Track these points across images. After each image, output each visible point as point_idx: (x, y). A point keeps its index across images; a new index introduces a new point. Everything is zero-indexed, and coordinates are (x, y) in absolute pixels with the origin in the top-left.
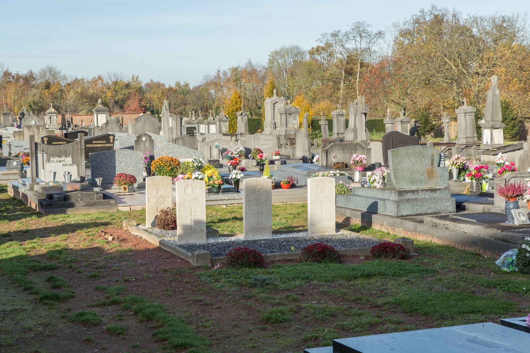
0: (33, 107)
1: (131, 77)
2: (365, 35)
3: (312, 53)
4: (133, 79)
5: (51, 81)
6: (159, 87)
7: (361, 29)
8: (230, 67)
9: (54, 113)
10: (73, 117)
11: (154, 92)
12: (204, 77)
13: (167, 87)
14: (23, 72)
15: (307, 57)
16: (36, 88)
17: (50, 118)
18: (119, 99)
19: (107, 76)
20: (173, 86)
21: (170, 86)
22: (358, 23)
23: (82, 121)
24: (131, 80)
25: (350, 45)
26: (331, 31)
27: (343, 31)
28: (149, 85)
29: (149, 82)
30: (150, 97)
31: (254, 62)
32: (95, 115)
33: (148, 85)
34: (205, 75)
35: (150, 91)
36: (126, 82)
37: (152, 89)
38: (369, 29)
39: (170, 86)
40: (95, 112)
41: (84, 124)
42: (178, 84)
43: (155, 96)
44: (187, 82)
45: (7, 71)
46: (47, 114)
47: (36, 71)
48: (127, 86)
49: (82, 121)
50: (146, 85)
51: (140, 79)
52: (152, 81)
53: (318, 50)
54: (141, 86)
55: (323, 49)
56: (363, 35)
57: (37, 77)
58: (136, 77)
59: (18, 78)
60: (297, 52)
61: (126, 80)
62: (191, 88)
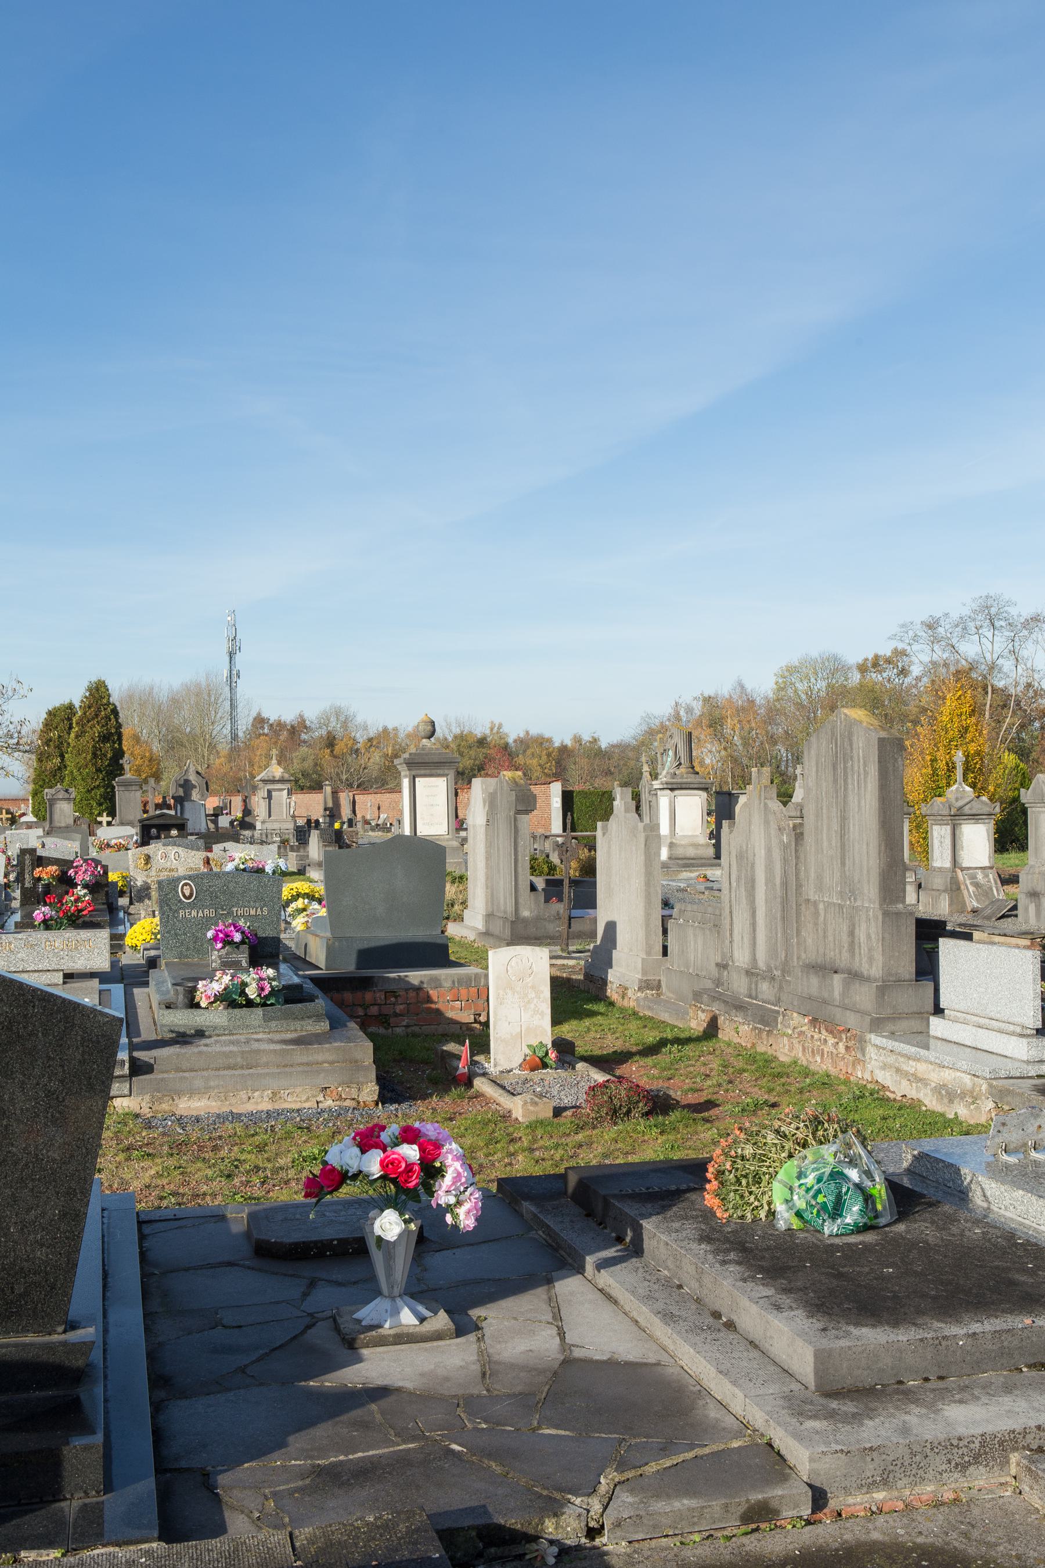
0: (302, 782)
1: (489, 725)
2: (1003, 623)
3: (862, 668)
4: (492, 729)
5: (339, 733)
6: (541, 743)
7: (993, 611)
8: (697, 694)
9: (282, 781)
10: (357, 797)
11: (533, 754)
12: (642, 718)
13: (557, 744)
14: (289, 717)
15: (856, 677)
16: (309, 746)
17: (270, 797)
18: (465, 768)
19: (444, 724)
20: (568, 742)
21: (562, 742)
22: (987, 597)
23: (379, 808)
24: (488, 732)
25: (970, 649)
26: (925, 617)
27: (955, 616)
28: (521, 742)
29: (522, 735)
30: (525, 764)
31: (749, 686)
32: (406, 783)
33: (520, 741)
34: (644, 715)
35: (525, 751)
36: (479, 736)
37: (528, 747)
38: (1013, 611)
39: (562, 742)
40: (404, 771)
41: (383, 816)
42: (577, 740)
43: (535, 761)
44: (596, 736)
45: (259, 714)
46: (261, 785)
47: (312, 714)
48: (482, 742)
49: (379, 808)
50: (515, 741)
51: (505, 729)
52: (527, 733)
53: (876, 663)
54: (507, 744)
55: (888, 661)
56: (997, 624)
57: (313, 726)
58: (497, 725)
59: (280, 725)
60: (835, 667)
61: (479, 731)
62: (603, 747)
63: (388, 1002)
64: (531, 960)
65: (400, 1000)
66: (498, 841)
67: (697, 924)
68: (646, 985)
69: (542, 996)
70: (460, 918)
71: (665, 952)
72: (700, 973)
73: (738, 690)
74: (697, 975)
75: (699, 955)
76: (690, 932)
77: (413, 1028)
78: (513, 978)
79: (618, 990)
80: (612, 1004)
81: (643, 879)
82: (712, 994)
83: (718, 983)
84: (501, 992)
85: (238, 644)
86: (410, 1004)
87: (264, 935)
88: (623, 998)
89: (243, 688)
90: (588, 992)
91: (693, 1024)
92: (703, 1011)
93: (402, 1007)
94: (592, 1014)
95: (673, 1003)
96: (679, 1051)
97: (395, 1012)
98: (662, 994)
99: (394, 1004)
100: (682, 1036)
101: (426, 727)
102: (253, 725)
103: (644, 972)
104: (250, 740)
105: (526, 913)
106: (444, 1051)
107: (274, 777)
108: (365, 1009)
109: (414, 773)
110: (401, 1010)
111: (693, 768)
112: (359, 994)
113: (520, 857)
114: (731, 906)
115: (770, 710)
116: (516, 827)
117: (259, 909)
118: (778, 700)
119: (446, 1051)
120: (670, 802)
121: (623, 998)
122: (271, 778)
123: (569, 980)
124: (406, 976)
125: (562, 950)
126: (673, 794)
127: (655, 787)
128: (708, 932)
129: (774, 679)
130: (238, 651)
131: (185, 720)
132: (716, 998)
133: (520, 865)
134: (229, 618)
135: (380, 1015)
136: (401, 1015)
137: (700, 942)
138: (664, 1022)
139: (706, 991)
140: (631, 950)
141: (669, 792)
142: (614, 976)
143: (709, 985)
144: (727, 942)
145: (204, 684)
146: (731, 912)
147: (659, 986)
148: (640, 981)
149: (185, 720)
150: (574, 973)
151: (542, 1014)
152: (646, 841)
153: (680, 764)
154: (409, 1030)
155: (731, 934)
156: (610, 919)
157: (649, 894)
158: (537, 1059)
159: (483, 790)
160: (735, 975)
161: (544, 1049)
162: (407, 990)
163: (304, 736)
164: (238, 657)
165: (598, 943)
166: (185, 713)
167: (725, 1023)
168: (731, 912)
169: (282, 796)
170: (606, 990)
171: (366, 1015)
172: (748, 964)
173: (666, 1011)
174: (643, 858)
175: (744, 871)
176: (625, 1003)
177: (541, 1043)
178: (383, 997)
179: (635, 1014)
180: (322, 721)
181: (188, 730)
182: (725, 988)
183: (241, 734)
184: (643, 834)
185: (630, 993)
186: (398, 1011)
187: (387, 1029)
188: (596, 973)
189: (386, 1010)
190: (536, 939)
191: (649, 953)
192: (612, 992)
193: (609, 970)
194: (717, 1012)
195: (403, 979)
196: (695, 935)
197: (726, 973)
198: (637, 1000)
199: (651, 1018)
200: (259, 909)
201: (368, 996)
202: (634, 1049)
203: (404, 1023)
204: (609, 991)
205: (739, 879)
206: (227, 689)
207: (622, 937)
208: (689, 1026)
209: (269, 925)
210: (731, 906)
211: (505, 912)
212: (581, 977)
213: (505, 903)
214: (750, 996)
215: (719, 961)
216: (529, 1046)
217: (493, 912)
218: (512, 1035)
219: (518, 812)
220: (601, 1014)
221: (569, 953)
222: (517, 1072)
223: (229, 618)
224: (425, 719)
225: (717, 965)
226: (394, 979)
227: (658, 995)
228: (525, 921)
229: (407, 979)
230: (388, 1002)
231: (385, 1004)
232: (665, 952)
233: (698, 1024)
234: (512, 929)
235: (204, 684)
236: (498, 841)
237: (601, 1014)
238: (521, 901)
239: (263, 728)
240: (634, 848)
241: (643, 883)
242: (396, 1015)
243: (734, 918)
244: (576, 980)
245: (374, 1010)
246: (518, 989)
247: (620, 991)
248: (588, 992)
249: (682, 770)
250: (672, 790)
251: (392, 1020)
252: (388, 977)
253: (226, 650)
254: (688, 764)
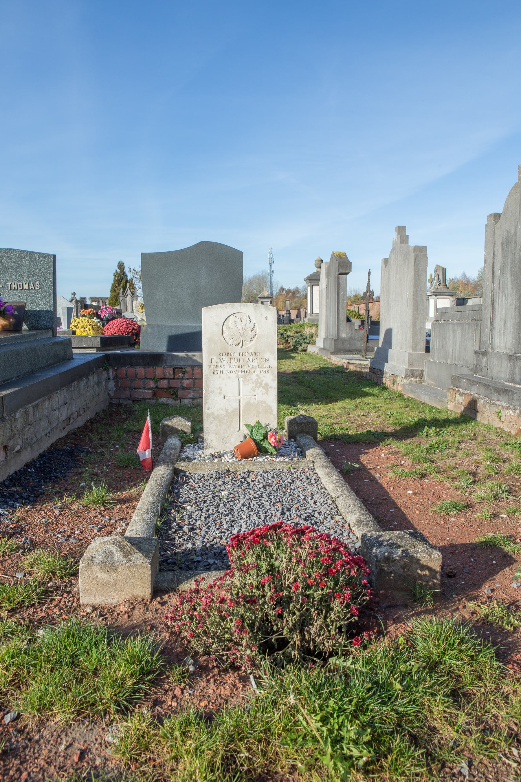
14: (292, 287)
31: (468, 275)
46: (259, 299)
59: (289, 291)
63: (176, 377)
64: (253, 320)
65: (186, 376)
67: (456, 321)
68: (411, 374)
69: (266, 365)
70: (314, 343)
71: (428, 350)
72: (456, 363)
73: (464, 276)
74: (455, 364)
75: (457, 348)
76: (450, 329)
78: (230, 342)
79: (391, 378)
80: (386, 389)
81: (412, 290)
82: (471, 378)
83: (476, 369)
84: (215, 359)
86: (195, 379)
87: (38, 309)
88: (393, 384)
89: (275, 276)
90: (371, 381)
91: (450, 406)
92: (461, 394)
93: (188, 381)
94: (367, 395)
95: (433, 388)
96: (437, 434)
97: (182, 386)
98: (423, 381)
99: (181, 379)
100: (441, 417)
103: (410, 364)
105: (343, 335)
106: (165, 426)
108: (156, 382)
110: (187, 384)
111: (446, 285)
112: (150, 369)
113: (341, 301)
114: (493, 295)
115: (475, 285)
116: (339, 283)
117: (32, 284)
118: (479, 281)
119: (168, 426)
120: (435, 301)
121: (393, 384)
123: (360, 372)
124: (194, 356)
125: (363, 356)
126: (436, 298)
127: (428, 294)
128: (466, 326)
129: (478, 273)
132: (474, 382)
133: (340, 306)
135: (169, 388)
136: (187, 389)
137: (458, 336)
138: (423, 403)
139: (464, 377)
140: (401, 348)
141: (434, 296)
142: (388, 368)
143: (466, 371)
144: (487, 331)
145: (261, 275)
146: (493, 302)
147: (421, 375)
148: (407, 370)
150: (364, 368)
151: (266, 387)
152: (415, 259)
153: (440, 284)
155: (492, 323)
156: (388, 327)
157: (417, 301)
158: (253, 444)
160: (495, 361)
161: (263, 431)
163: (298, 295)
164: (273, 265)
165: (380, 346)
167: (485, 407)
168: (493, 302)
170: (383, 378)
171: (157, 387)
172: (511, 351)
173: (426, 394)
174: (412, 273)
175: (510, 257)
176: (395, 388)
177: (258, 423)
178: (172, 372)
179: (401, 396)
182: (483, 373)
183: (274, 294)
184: (413, 255)
185: (398, 380)
186: (185, 385)
187: (175, 400)
188: (377, 367)
189: (175, 384)
190: (349, 351)
191: (414, 349)
192: (387, 381)
193: (385, 364)
194: (476, 396)
196: (454, 331)
197: (485, 359)
198: (403, 385)
199: (414, 400)
200: (32, 284)
201: (159, 371)
202: (390, 429)
203: (191, 396)
204: (384, 379)
205: (504, 266)
207: (396, 339)
208: (447, 408)
209: (42, 299)
210: (493, 295)
212: (368, 371)
214: (513, 381)
215: (477, 349)
216: (248, 426)
218: (227, 411)
219: (340, 273)
220: (373, 395)
221: (366, 358)
222: (227, 458)
225: (476, 352)
226: (182, 358)
227: (421, 382)
228: (343, 340)
229: (194, 358)
230: (176, 377)
231: (174, 378)
232: (428, 350)
233: (455, 407)
234: (335, 344)
235: (261, 275)
237: (373, 395)
238: (341, 327)
240: (406, 268)
241: (412, 294)
242: (183, 388)
243: (496, 305)
244: (365, 372)
245: (164, 384)
246: (237, 356)
247: (392, 379)
248: (371, 381)
249: (441, 286)
250: (436, 295)
251: (180, 393)
252: (177, 356)
254: (444, 284)
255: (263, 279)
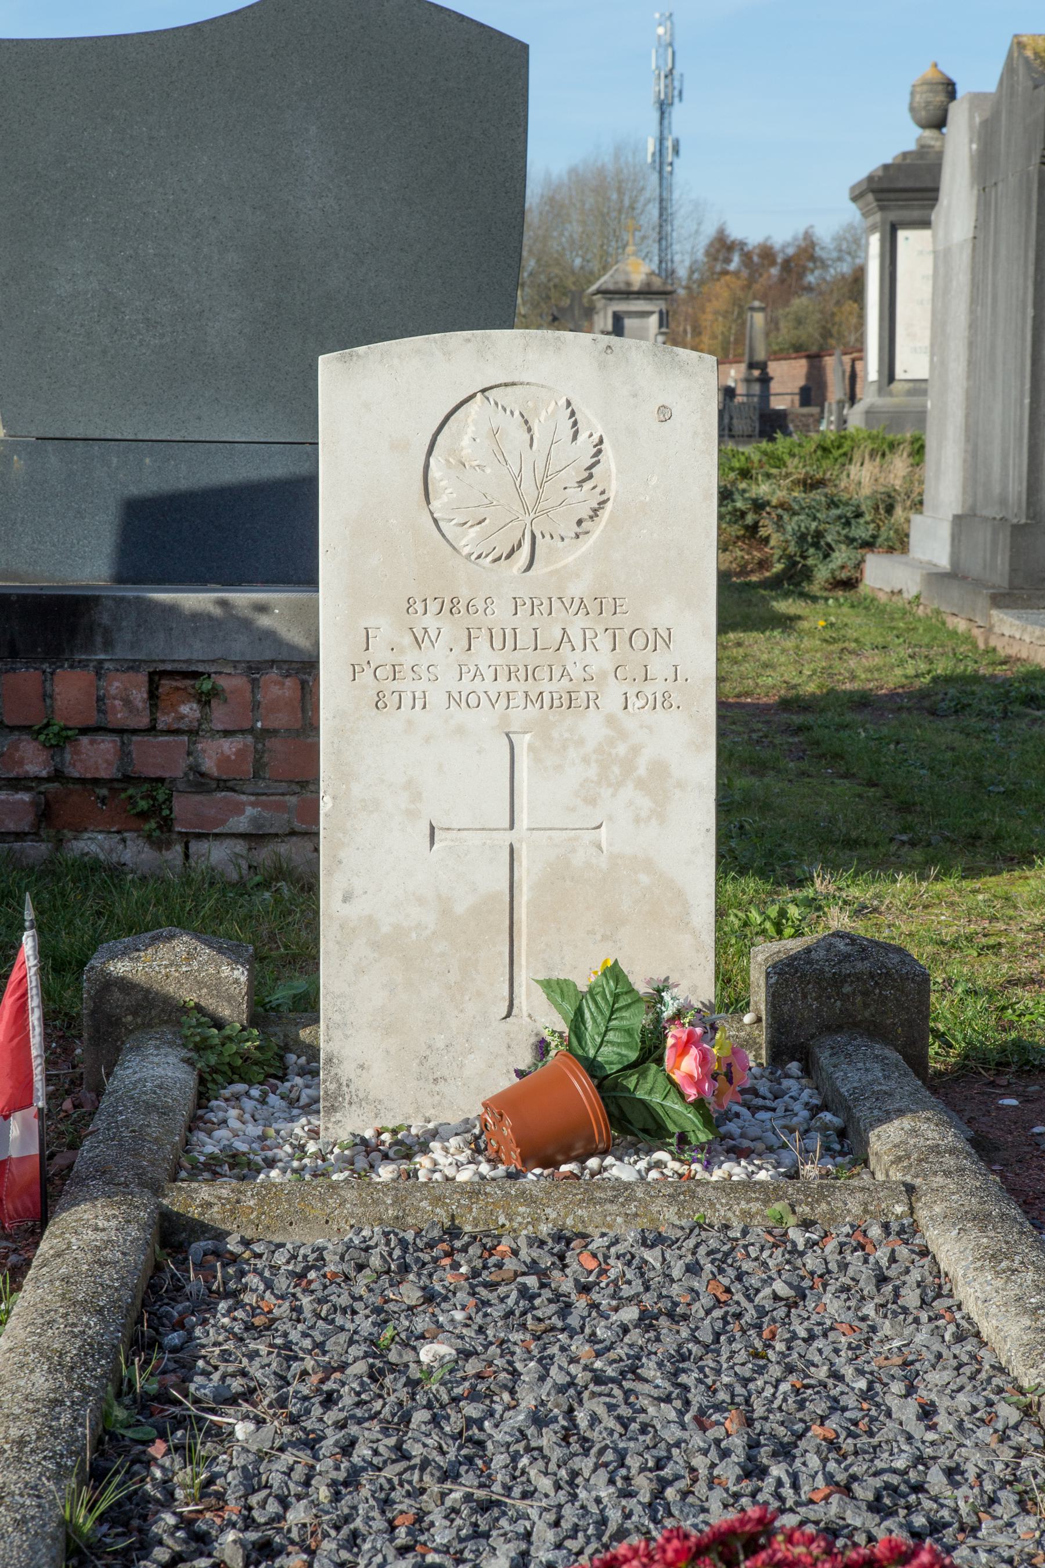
59: (767, 254)
63: (164, 720)
64: (593, 424)
65: (220, 716)
66: (995, 272)
69: (659, 664)
70: (899, 544)
77: (283, 848)
78: (468, 540)
85: (677, 84)
86: (267, 732)
93: (229, 746)
97: (195, 770)
99: (193, 733)
101: (930, 97)
102: (707, 253)
104: (701, 283)
106: (110, 984)
107: (628, 284)
109: (893, 216)
110: (224, 761)
119: (125, 985)
122: (622, 286)
130: (676, 100)
131: (572, 242)
134: (661, 31)
135: (128, 779)
136: (223, 785)
149: (572, 242)
154: (265, 854)
158: (582, 1086)
159: (971, 127)
161: (639, 1019)
162: (254, 670)
163: (811, 278)
164: (678, 113)
166: (574, 229)
169: (646, 329)
171: (58, 775)
177: (614, 972)
178: (139, 696)
180: (844, 246)
181: (578, 262)
183: (682, 272)
186: (209, 765)
187: (159, 845)
195: (246, 624)
203: (241, 823)
206: (654, 177)
211: (1003, 502)
213: (1005, 475)
217: (973, 508)
223: (661, 31)
224: (937, 78)
226: (197, 618)
230: (164, 720)
231: (152, 729)
236: (995, 272)
239: (728, 261)
253: (652, 99)
255: (620, 191)
